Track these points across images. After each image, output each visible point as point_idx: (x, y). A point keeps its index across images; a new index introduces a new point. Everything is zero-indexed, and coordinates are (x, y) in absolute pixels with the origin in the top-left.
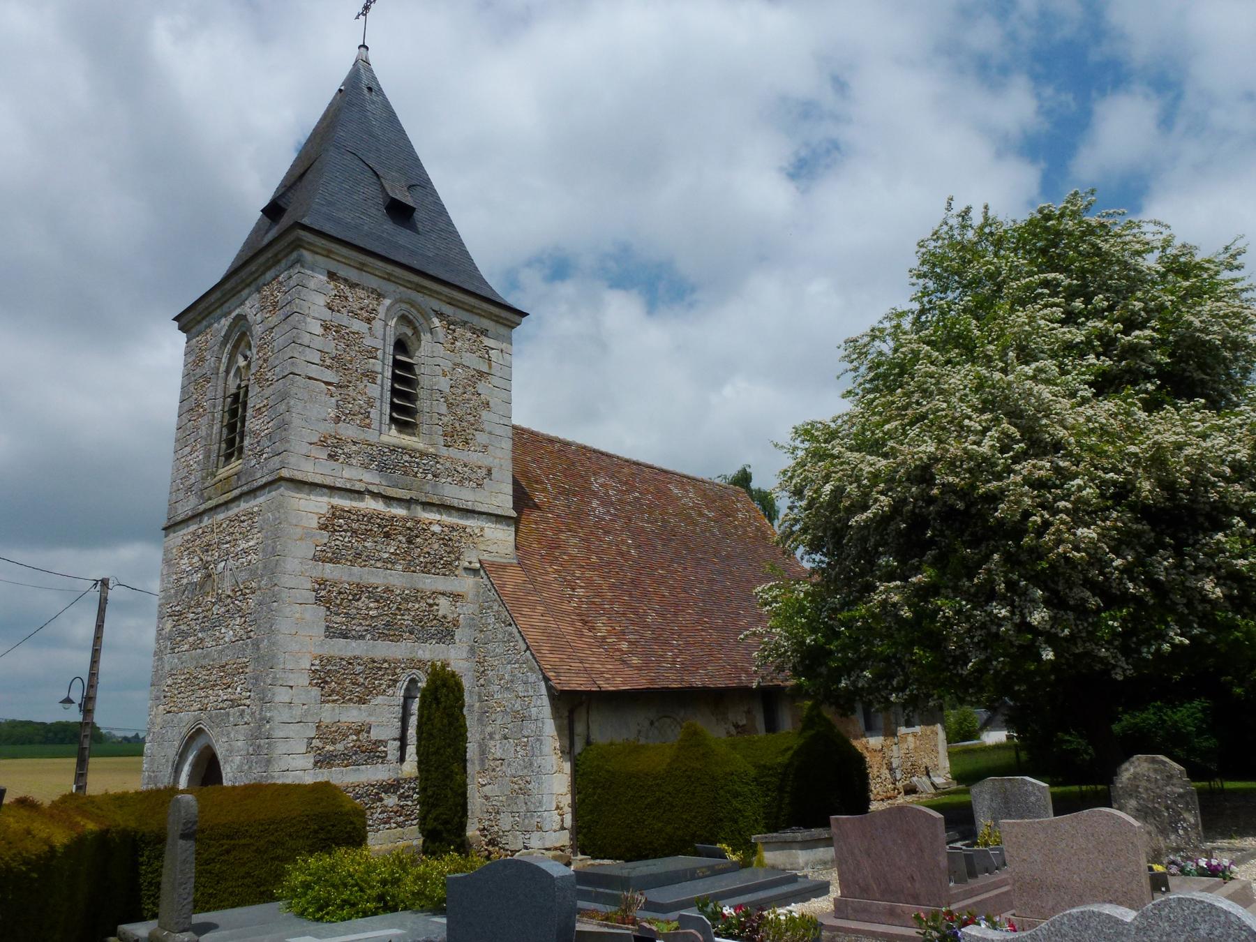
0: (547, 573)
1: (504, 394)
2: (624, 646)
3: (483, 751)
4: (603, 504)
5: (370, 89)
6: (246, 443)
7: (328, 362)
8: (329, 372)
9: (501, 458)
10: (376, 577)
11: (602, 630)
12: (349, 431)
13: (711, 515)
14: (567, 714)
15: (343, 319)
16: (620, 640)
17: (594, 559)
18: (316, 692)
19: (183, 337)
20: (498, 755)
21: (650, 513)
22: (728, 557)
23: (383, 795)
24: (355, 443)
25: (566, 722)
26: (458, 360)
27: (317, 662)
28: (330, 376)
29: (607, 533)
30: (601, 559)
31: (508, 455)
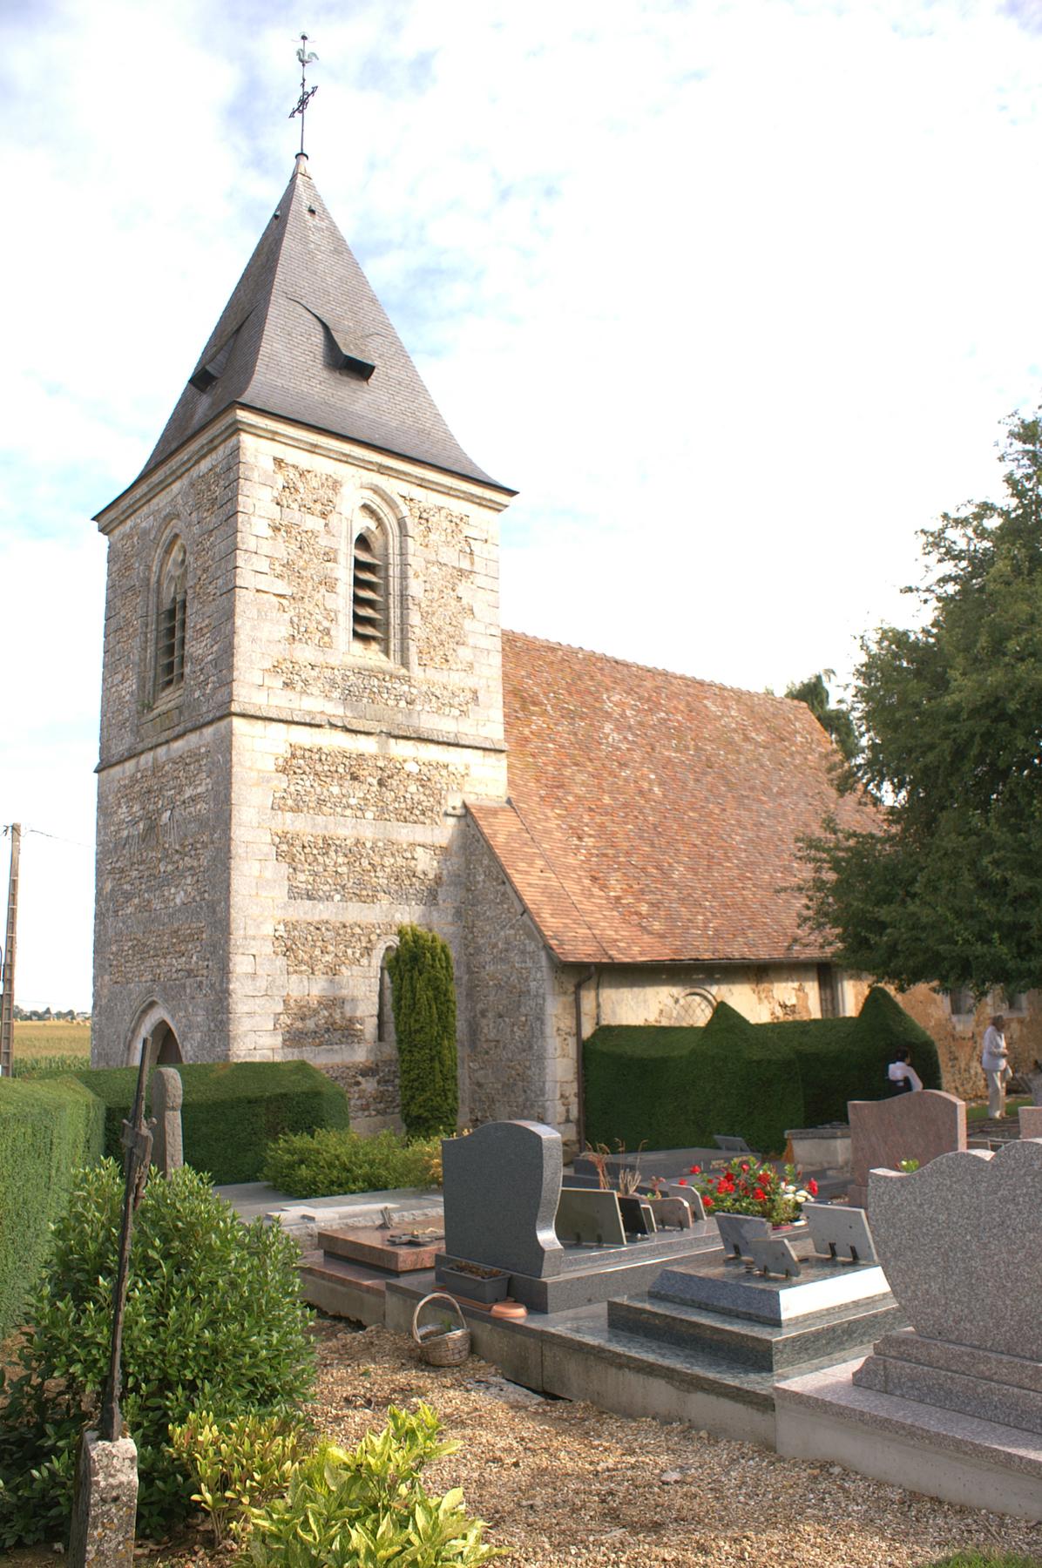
0: (547, 819)
1: (491, 597)
2: (644, 908)
3: (474, 1030)
4: (618, 729)
5: (312, 212)
6: (187, 670)
7: (279, 569)
8: (279, 581)
9: (489, 673)
10: (345, 829)
11: (616, 886)
12: (306, 653)
13: (760, 738)
14: (572, 989)
15: (294, 515)
16: (639, 900)
17: (607, 800)
18: (281, 962)
19: (104, 541)
20: (492, 1035)
21: (680, 739)
22: (782, 793)
23: (360, 1078)
24: (313, 667)
25: (572, 998)
26: (433, 557)
27: (281, 927)
28: (282, 587)
29: (622, 765)
30: (615, 799)
31: (496, 672)
